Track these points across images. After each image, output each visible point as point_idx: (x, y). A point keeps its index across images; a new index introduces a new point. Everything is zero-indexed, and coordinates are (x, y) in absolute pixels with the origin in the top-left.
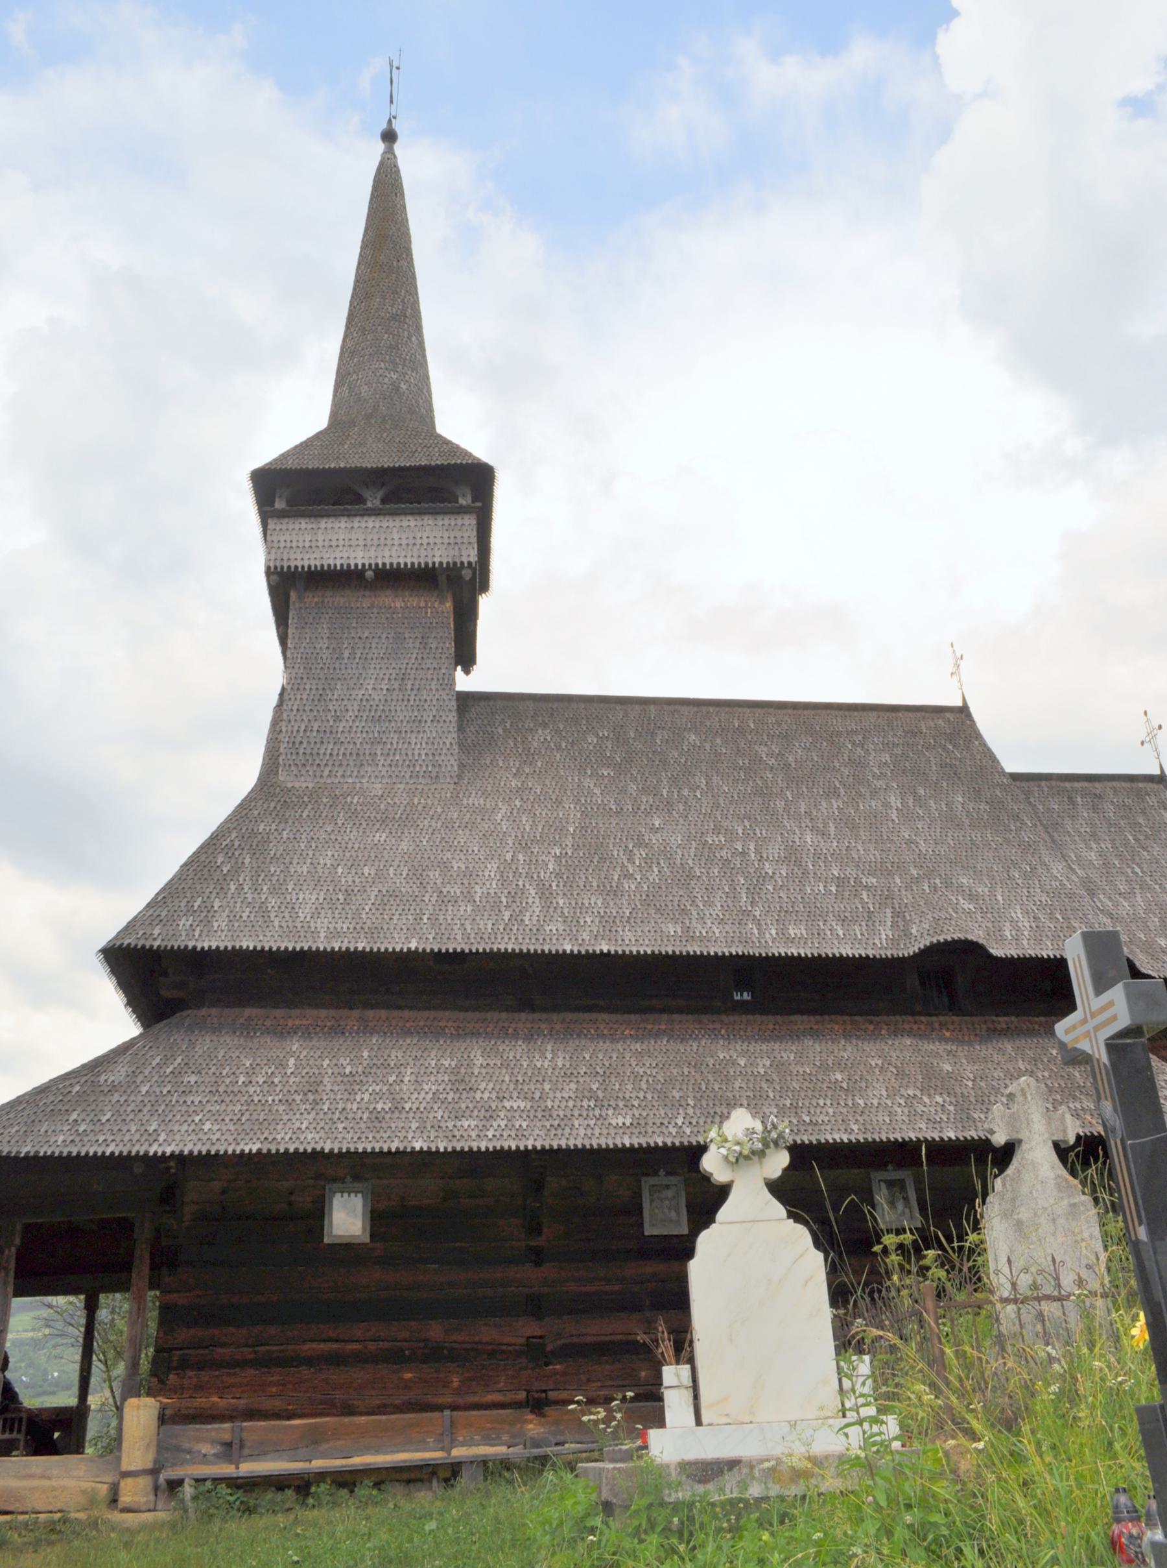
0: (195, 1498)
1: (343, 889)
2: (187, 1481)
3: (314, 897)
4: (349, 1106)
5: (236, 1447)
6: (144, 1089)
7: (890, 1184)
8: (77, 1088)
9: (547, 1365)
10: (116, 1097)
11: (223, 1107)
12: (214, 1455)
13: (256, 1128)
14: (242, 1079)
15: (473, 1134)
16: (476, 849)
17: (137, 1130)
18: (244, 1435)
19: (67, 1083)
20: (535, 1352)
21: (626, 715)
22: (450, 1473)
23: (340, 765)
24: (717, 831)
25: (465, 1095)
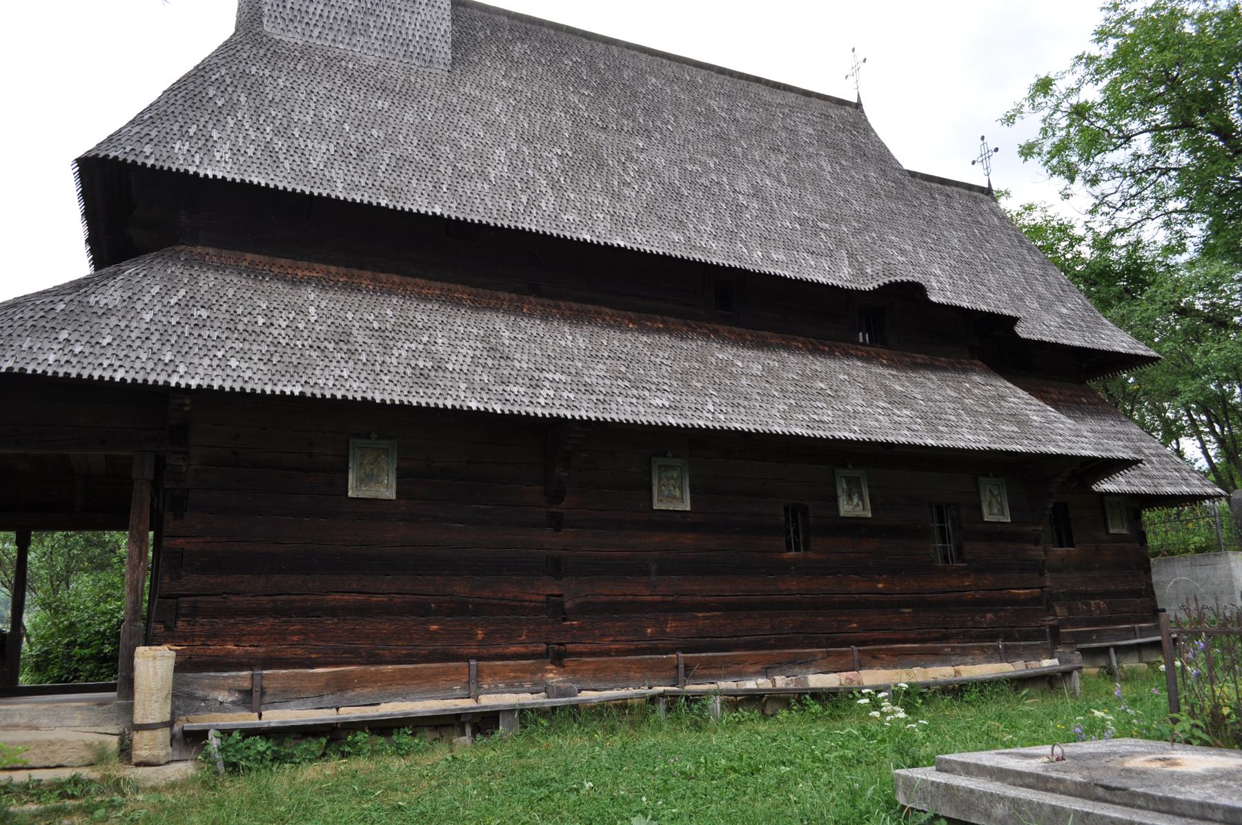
0: (221, 750)
1: (354, 145)
2: (211, 734)
3: (324, 148)
4: (388, 360)
5: (256, 695)
6: (148, 318)
7: (849, 480)
8: (61, 306)
9: (564, 620)
10: (113, 321)
11: (247, 346)
12: (233, 702)
13: (292, 370)
14: (261, 321)
15: (526, 400)
16: (482, 134)
17: (148, 359)
18: (265, 683)
19: (47, 300)
20: (555, 609)
21: (593, 48)
22: (485, 722)
23: (331, 28)
24: (693, 161)
25: (503, 362)
